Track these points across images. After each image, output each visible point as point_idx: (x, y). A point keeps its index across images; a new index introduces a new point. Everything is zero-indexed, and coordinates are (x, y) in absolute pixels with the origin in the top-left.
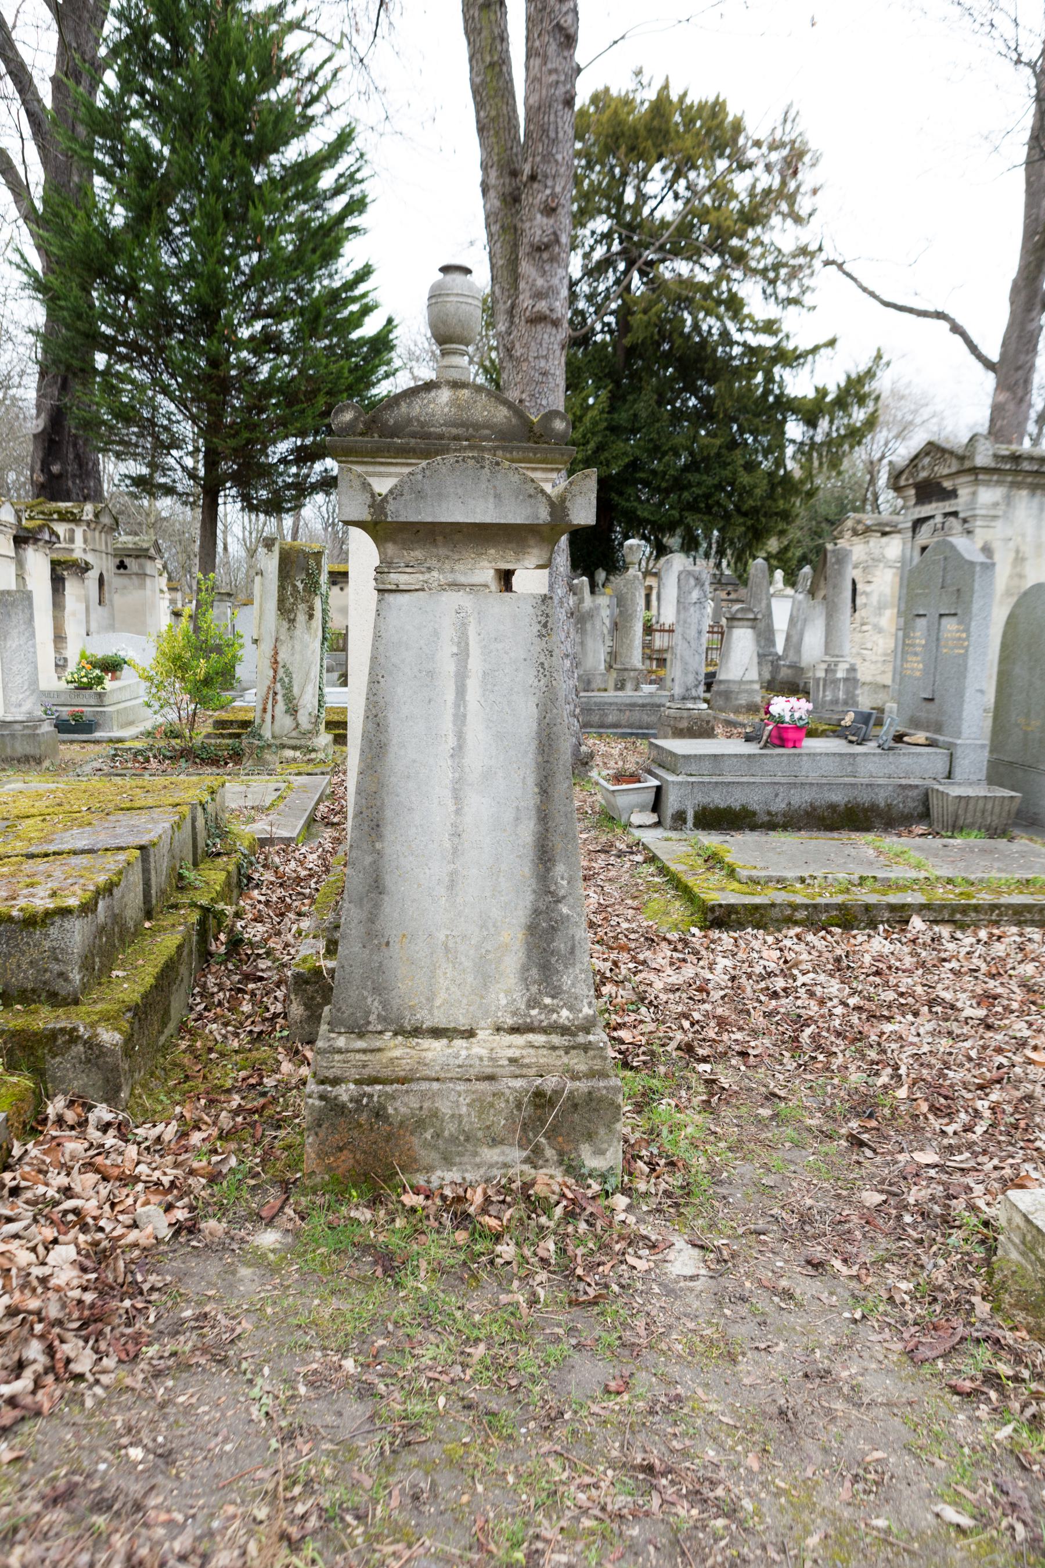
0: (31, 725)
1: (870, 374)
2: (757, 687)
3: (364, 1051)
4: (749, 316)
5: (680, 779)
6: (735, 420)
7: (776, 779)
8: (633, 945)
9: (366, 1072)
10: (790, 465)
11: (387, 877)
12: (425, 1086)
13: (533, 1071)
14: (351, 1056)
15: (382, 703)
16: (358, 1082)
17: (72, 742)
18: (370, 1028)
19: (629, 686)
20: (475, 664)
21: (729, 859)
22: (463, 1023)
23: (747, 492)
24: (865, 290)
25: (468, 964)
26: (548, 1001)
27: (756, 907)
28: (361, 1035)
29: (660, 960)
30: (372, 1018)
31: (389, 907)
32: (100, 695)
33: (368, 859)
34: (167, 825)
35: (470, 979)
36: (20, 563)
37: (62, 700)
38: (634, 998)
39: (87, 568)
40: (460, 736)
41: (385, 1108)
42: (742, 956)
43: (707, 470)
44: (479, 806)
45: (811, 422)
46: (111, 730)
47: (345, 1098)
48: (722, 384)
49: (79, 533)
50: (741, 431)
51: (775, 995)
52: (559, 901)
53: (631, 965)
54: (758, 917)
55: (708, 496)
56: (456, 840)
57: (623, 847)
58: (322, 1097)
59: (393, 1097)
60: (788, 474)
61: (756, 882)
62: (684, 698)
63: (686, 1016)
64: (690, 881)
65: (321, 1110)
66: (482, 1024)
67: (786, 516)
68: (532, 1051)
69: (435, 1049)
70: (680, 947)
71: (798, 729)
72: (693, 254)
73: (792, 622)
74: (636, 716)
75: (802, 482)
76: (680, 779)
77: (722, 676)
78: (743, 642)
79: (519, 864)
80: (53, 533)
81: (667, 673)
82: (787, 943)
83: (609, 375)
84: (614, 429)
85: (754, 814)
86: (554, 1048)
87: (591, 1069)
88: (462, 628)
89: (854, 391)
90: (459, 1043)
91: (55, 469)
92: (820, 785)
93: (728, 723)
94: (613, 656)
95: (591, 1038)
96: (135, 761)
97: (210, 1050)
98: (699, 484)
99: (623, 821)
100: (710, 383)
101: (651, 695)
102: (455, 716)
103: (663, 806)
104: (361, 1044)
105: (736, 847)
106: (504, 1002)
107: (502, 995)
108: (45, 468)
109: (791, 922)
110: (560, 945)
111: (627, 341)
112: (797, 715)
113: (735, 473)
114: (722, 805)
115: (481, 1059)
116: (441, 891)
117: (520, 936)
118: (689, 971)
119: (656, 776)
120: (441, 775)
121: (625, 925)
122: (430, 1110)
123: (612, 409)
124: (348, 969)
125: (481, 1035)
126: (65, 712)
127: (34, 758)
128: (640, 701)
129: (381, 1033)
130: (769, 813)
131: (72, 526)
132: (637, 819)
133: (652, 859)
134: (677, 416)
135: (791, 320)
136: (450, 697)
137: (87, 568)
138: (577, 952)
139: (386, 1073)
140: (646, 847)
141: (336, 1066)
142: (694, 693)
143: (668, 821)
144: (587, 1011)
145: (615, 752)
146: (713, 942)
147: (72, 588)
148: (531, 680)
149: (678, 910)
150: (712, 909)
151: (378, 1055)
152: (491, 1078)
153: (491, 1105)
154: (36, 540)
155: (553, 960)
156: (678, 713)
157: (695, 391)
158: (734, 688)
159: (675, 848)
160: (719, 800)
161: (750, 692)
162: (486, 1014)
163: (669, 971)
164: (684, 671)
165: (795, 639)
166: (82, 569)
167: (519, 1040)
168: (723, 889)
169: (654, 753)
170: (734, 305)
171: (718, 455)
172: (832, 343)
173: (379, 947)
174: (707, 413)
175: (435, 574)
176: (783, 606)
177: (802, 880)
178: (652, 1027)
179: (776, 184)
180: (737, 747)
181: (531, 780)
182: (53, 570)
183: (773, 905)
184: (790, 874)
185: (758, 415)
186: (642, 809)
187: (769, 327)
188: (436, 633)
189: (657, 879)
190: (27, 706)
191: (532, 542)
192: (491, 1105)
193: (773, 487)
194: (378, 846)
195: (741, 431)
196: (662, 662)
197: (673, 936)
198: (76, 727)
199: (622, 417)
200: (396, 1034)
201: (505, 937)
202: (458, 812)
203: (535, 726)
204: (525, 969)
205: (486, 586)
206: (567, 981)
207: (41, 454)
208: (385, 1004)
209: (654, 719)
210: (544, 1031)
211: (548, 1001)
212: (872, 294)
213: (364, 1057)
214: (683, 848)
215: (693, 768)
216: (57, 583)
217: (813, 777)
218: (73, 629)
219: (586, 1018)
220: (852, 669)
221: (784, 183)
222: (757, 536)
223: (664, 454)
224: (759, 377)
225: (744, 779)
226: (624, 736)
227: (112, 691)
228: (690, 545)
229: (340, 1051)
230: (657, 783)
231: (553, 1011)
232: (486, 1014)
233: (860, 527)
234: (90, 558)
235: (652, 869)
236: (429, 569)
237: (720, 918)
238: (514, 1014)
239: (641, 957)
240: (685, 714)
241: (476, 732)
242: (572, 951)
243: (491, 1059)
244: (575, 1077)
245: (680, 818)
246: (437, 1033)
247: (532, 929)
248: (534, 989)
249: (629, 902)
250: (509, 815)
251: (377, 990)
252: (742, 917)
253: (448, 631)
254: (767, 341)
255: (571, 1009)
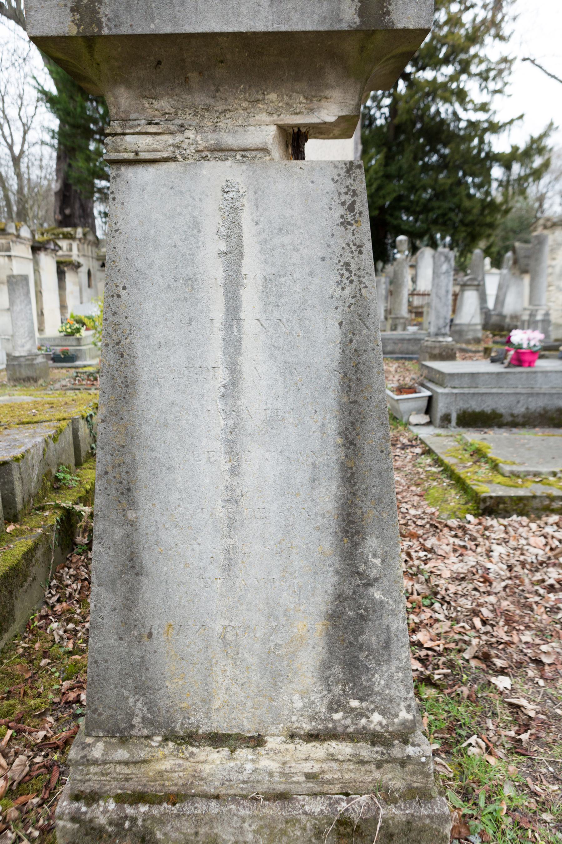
0: (31, 358)
1: (545, 135)
2: (479, 327)
3: (126, 763)
4: (471, 101)
5: (447, 390)
6: (461, 168)
7: (518, 390)
8: (420, 532)
9: (130, 787)
10: (494, 192)
11: (145, 556)
12: (201, 806)
13: (336, 788)
14: (110, 768)
15: (125, 325)
16: (120, 799)
17: (62, 368)
18: (134, 732)
19: (400, 328)
20: (252, 266)
21: (491, 454)
22: (249, 728)
23: (467, 212)
24: (549, 74)
25: (252, 660)
26: (354, 703)
27: (520, 499)
28: (124, 741)
29: (444, 547)
30: (136, 721)
31: (150, 593)
32: (78, 340)
33: (119, 533)
34: (39, 439)
35: (256, 678)
36: (36, 263)
37: (57, 342)
38: (428, 592)
39: (79, 266)
40: (234, 368)
41: (152, 833)
42: (513, 543)
43: (444, 199)
44: (262, 463)
45: (508, 167)
46: (85, 360)
47: (102, 820)
48: (453, 145)
49: (75, 245)
50: (465, 175)
51: (551, 589)
52: (369, 585)
53: (422, 554)
54: (522, 506)
55: (444, 215)
56: (233, 508)
57: (405, 441)
58: (74, 819)
59: (161, 821)
60: (493, 201)
61: (517, 475)
62: (437, 335)
63: (476, 613)
64: (461, 472)
65: (74, 833)
66: (273, 729)
67: (491, 226)
68: (335, 765)
69: (213, 762)
70: (460, 534)
71: (533, 353)
72: (436, 64)
73: (500, 287)
74: (405, 346)
75: (501, 204)
76: (447, 390)
77: (457, 321)
78: (470, 298)
79: (317, 540)
80: (56, 244)
81: (424, 320)
82: (549, 530)
83: (384, 144)
84: (388, 177)
85: (501, 416)
86: (363, 762)
87: (410, 788)
88: (233, 213)
89: (536, 147)
90: (243, 753)
91: (67, 211)
92: (551, 395)
93: (462, 350)
94: (388, 312)
95: (410, 750)
96: (88, 380)
97: (45, 655)
98: (439, 208)
99: (404, 420)
100: (445, 146)
101: (414, 333)
102: (226, 340)
103: (433, 410)
104: (122, 754)
105: (491, 440)
106: (299, 704)
107: (296, 697)
108: (62, 211)
109: (550, 511)
110: (371, 637)
111: (396, 121)
112: (532, 343)
113: (461, 200)
114: (478, 410)
115: (271, 774)
116: (215, 571)
117: (319, 627)
118: (471, 559)
119: (428, 388)
120: (210, 422)
121: (413, 512)
122: (207, 835)
123: (386, 165)
124: (103, 665)
125: (272, 743)
126: (58, 349)
127: (33, 379)
128: (407, 337)
129: (148, 737)
130: (512, 415)
131: (71, 241)
132: (414, 419)
133: (428, 452)
134: (426, 167)
135: (497, 102)
136: (218, 313)
137: (79, 266)
138: (394, 646)
139: (154, 787)
140: (422, 442)
141: (93, 779)
142: (443, 331)
143: (438, 421)
144: (404, 715)
145: (393, 369)
146: (486, 529)
147: (69, 277)
148: (332, 288)
149: (454, 498)
150: (484, 500)
151: (144, 768)
152: (283, 797)
153: (284, 832)
154: (46, 249)
155: (362, 656)
156: (433, 345)
157: (437, 152)
158: (465, 328)
159: (447, 442)
160: (475, 406)
161: (475, 331)
162: (277, 718)
163: (453, 558)
164: (433, 320)
165: (501, 298)
166: (77, 266)
167: (318, 750)
168: (490, 482)
169: (425, 372)
170: (461, 95)
171: (451, 189)
172: (521, 117)
173: (139, 639)
174: (444, 164)
175: (190, 134)
176: (492, 281)
177: (554, 474)
178: (445, 626)
179: (490, 15)
180: (483, 366)
181: (333, 427)
182: (58, 268)
183: (534, 497)
184: (545, 469)
185: (475, 164)
186: (418, 412)
187: (484, 107)
188: (195, 224)
189: (434, 469)
190: (28, 347)
191: (331, 78)
192: (284, 832)
193: (483, 208)
194: (131, 515)
195: (465, 175)
196: (419, 314)
197: (453, 522)
198: (65, 358)
199: (393, 169)
200: (166, 739)
201: (300, 627)
202: (234, 471)
203: (337, 352)
204: (326, 666)
205: (265, 150)
206: (379, 681)
207: (59, 203)
208: (151, 706)
209: (415, 348)
210: (351, 738)
211: (354, 703)
212: (553, 77)
213: (126, 770)
214: (450, 444)
215: (456, 383)
216: (61, 274)
217: (545, 388)
218: (72, 302)
219: (404, 723)
220: (547, 314)
221: (494, 16)
222: (473, 239)
223: (417, 190)
224: (476, 141)
225: (494, 391)
226: (397, 359)
227: (86, 337)
228: (434, 245)
229: (95, 762)
230: (428, 393)
231: (362, 715)
232: (277, 718)
233: (549, 224)
234: (82, 260)
235: (429, 461)
236: (182, 128)
237: (490, 508)
238: (312, 718)
239: (428, 544)
240: (437, 345)
241: (256, 361)
242: (387, 645)
243: (282, 774)
244: (389, 798)
245: (446, 419)
246: (217, 740)
247: (334, 618)
248: (337, 690)
249: (413, 488)
250: (302, 475)
251: (140, 689)
252: (509, 506)
253: (212, 221)
254: (481, 116)
255: (384, 713)
